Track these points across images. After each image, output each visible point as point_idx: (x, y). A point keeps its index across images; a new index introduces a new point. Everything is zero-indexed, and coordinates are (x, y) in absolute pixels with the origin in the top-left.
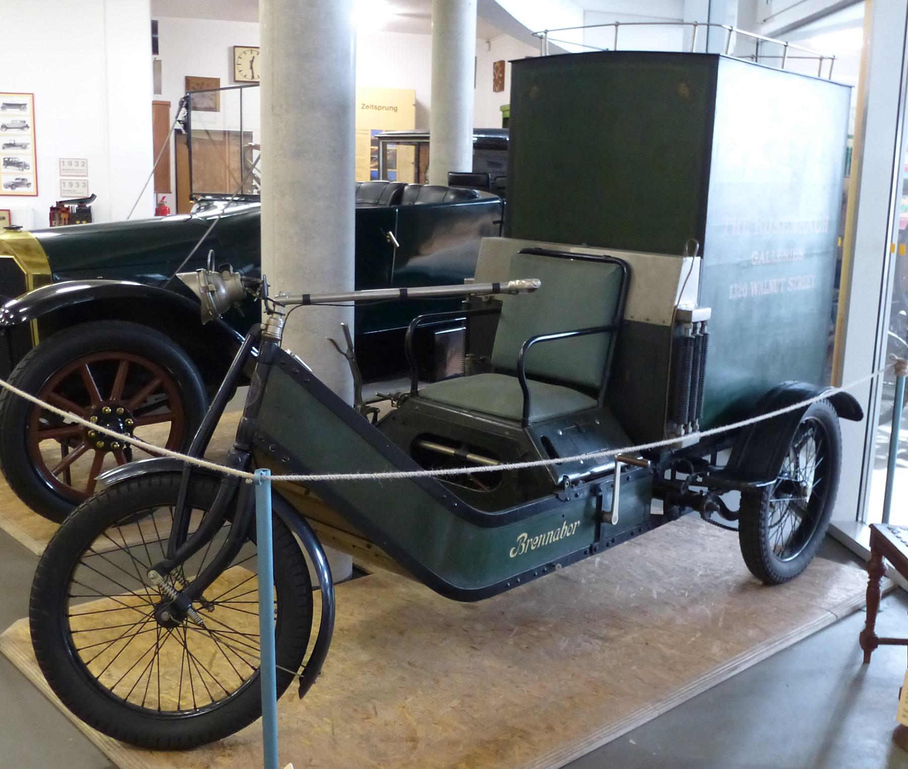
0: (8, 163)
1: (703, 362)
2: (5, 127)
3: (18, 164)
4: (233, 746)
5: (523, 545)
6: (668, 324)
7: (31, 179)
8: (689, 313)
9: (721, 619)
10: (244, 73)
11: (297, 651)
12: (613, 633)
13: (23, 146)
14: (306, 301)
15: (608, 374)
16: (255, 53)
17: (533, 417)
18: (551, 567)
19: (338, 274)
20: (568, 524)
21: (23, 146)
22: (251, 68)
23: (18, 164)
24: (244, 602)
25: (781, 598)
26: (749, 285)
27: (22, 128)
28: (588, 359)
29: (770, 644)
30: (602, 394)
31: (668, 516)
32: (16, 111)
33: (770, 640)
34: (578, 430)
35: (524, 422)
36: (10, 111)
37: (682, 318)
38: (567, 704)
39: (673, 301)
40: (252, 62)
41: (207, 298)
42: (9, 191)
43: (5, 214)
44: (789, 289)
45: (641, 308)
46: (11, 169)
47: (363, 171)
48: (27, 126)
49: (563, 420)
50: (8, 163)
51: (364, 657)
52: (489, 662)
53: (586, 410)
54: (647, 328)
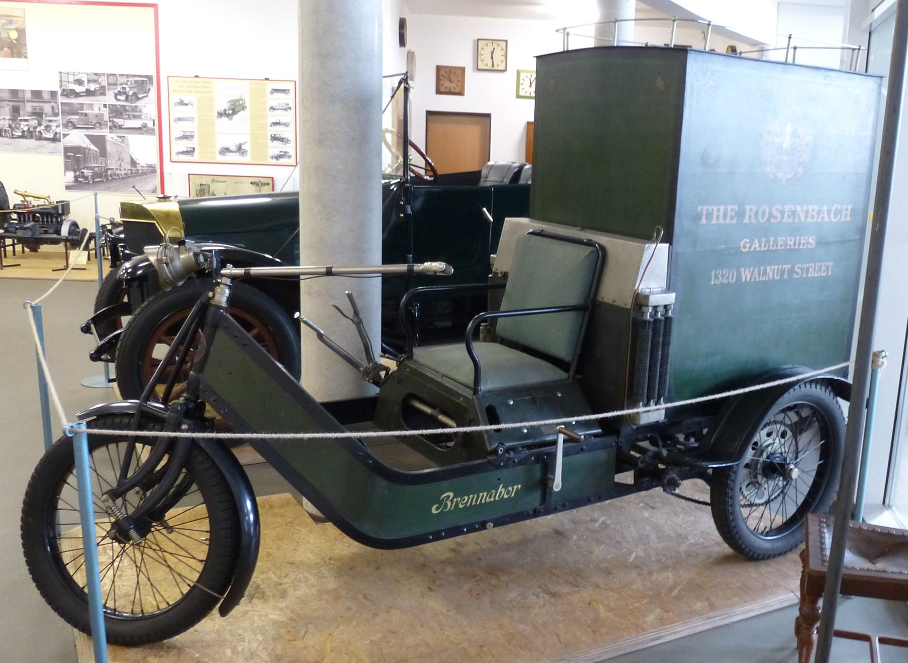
0: (274, 138)
1: (666, 344)
2: (272, 108)
3: (281, 140)
4: (170, 648)
5: (449, 503)
6: (629, 306)
7: (292, 152)
8: (647, 297)
9: (678, 589)
10: (485, 62)
11: (228, 573)
12: (565, 590)
13: (286, 125)
14: (329, 273)
15: (579, 350)
16: (495, 45)
17: (483, 387)
18: (483, 526)
19: (359, 248)
20: (505, 487)
21: (286, 125)
22: (492, 58)
23: (281, 140)
24: (189, 528)
25: (754, 574)
26: (739, 273)
27: (286, 110)
28: (559, 336)
29: (709, 618)
30: (573, 368)
31: (637, 487)
32: (282, 95)
33: (712, 614)
34: (534, 401)
35: (475, 391)
36: (277, 95)
37: (640, 301)
38: (473, 651)
39: (634, 285)
40: (492, 53)
41: (162, 268)
42: (274, 161)
43: (270, 181)
44: (795, 276)
45: (612, 292)
46: (276, 143)
47: (388, 161)
48: (290, 108)
49: (515, 392)
50: (274, 138)
51: (332, 584)
52: (435, 603)
53: (561, 380)
54: (614, 309)
